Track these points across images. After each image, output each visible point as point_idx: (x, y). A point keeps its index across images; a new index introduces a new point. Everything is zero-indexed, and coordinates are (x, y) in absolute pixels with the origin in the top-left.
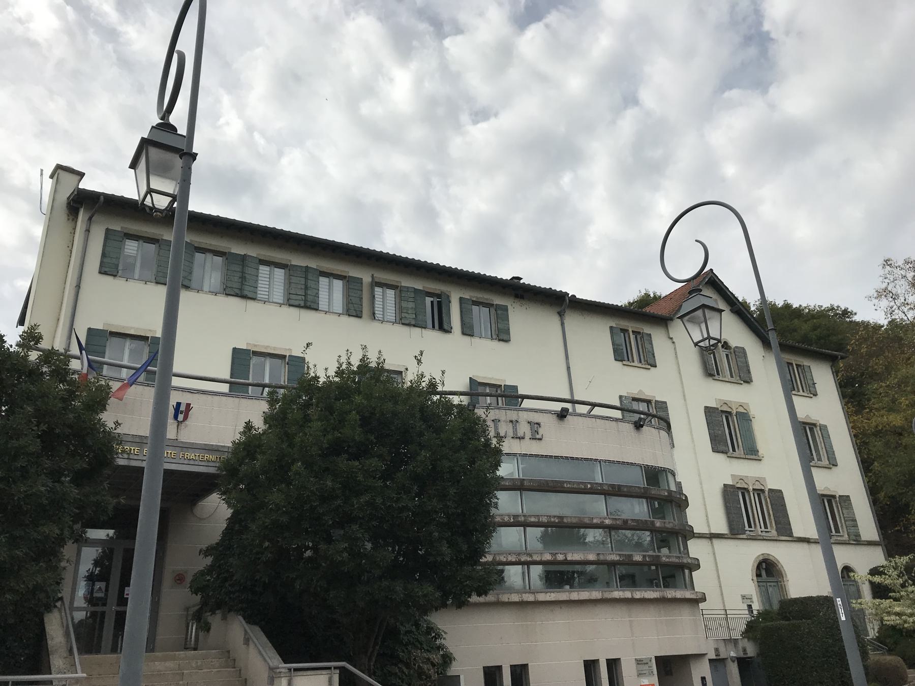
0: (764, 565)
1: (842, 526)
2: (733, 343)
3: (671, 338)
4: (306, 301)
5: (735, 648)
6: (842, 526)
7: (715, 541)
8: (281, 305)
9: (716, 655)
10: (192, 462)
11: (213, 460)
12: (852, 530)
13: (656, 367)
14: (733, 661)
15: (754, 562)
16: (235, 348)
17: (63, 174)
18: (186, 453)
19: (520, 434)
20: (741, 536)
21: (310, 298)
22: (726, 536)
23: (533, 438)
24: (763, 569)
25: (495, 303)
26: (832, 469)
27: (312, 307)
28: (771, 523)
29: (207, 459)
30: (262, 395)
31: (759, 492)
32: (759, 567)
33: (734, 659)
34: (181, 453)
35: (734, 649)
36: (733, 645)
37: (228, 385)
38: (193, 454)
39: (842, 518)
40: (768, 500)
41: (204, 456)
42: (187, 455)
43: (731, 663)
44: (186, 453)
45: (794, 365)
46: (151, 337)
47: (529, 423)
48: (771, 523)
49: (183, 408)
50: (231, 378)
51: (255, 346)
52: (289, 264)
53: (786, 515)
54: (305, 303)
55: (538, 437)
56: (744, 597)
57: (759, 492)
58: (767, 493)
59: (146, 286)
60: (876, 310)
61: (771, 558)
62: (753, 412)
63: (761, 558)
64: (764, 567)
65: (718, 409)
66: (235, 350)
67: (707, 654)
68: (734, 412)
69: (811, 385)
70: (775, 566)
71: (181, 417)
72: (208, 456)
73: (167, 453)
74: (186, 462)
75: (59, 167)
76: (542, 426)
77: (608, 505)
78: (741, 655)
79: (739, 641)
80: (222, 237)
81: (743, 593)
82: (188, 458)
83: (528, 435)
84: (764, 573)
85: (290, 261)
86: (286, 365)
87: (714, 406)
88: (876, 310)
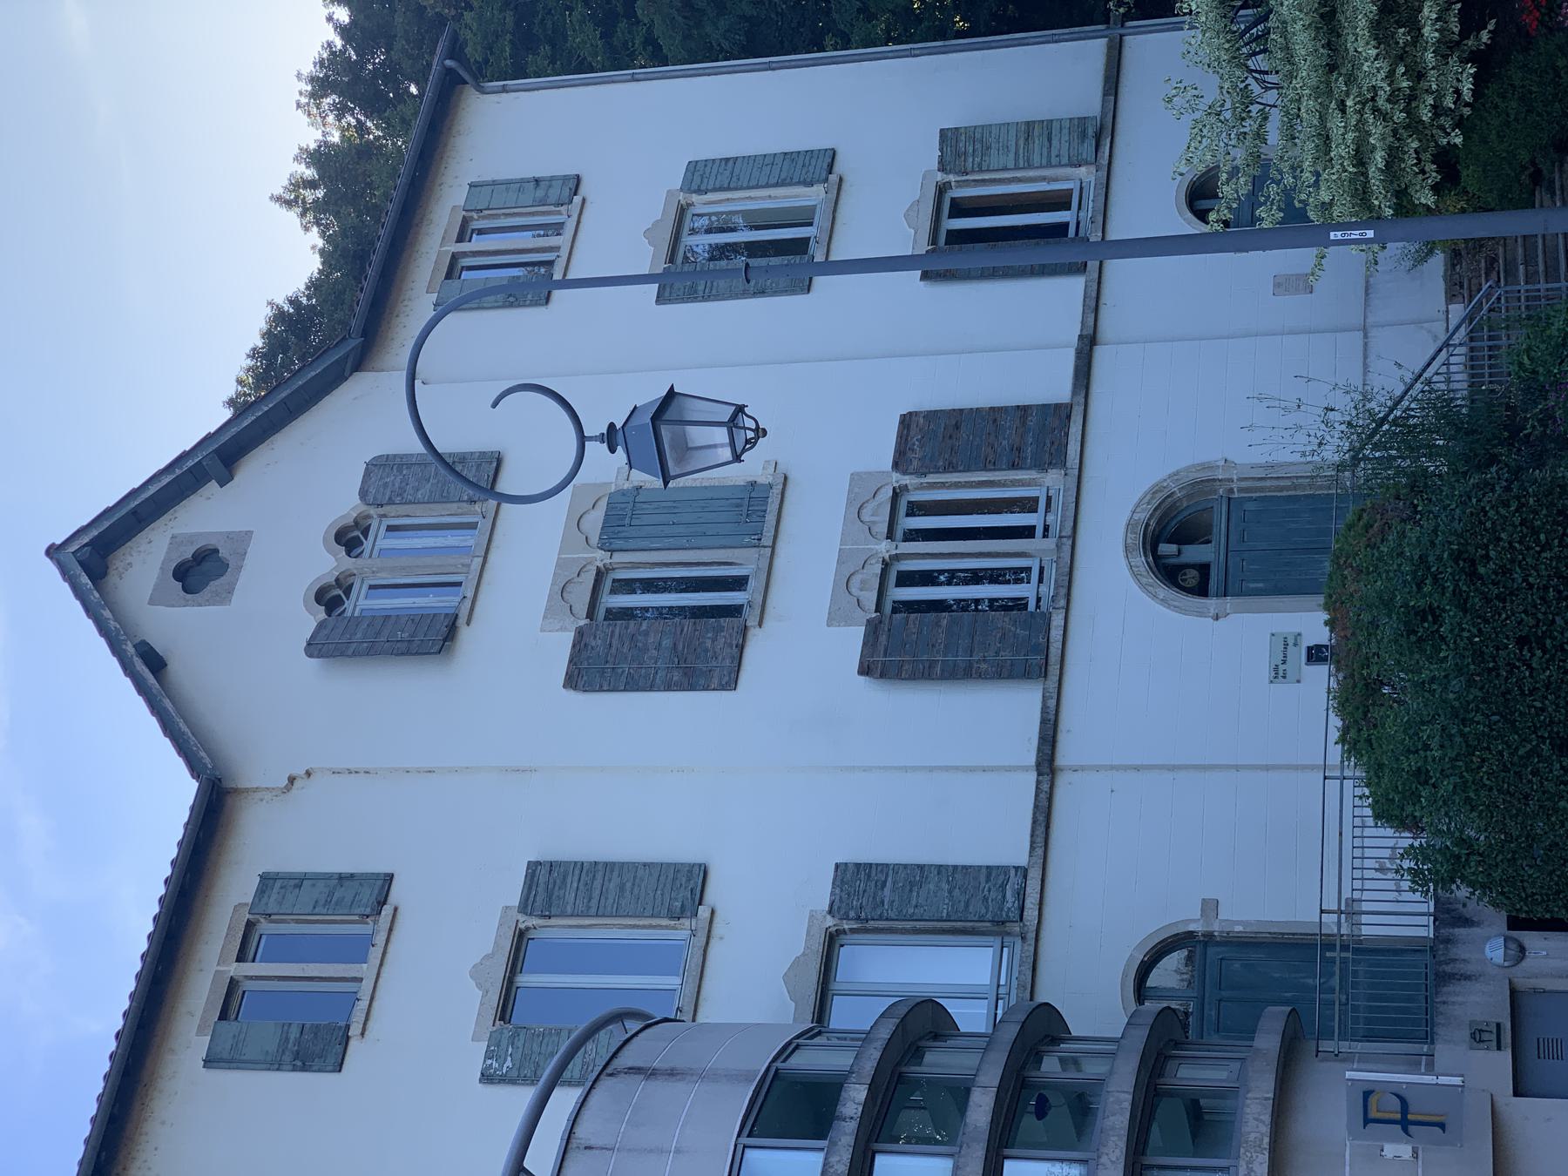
1: (1044, 179)
2: (346, 503)
3: (292, 780)
6: (1044, 179)
7: (1062, 759)
12: (1061, 144)
13: (389, 878)
20: (1056, 634)
31: (903, 509)
32: (1168, 573)
36: (1461, 932)
39: (1019, 174)
40: (932, 478)
45: (464, 247)
53: (994, 415)
56: (1278, 674)
57: (903, 509)
58: (907, 480)
63: (1140, 560)
65: (580, 633)
68: (600, 558)
69: (540, 193)
81: (1265, 672)
84: (1194, 553)
87: (568, 638)
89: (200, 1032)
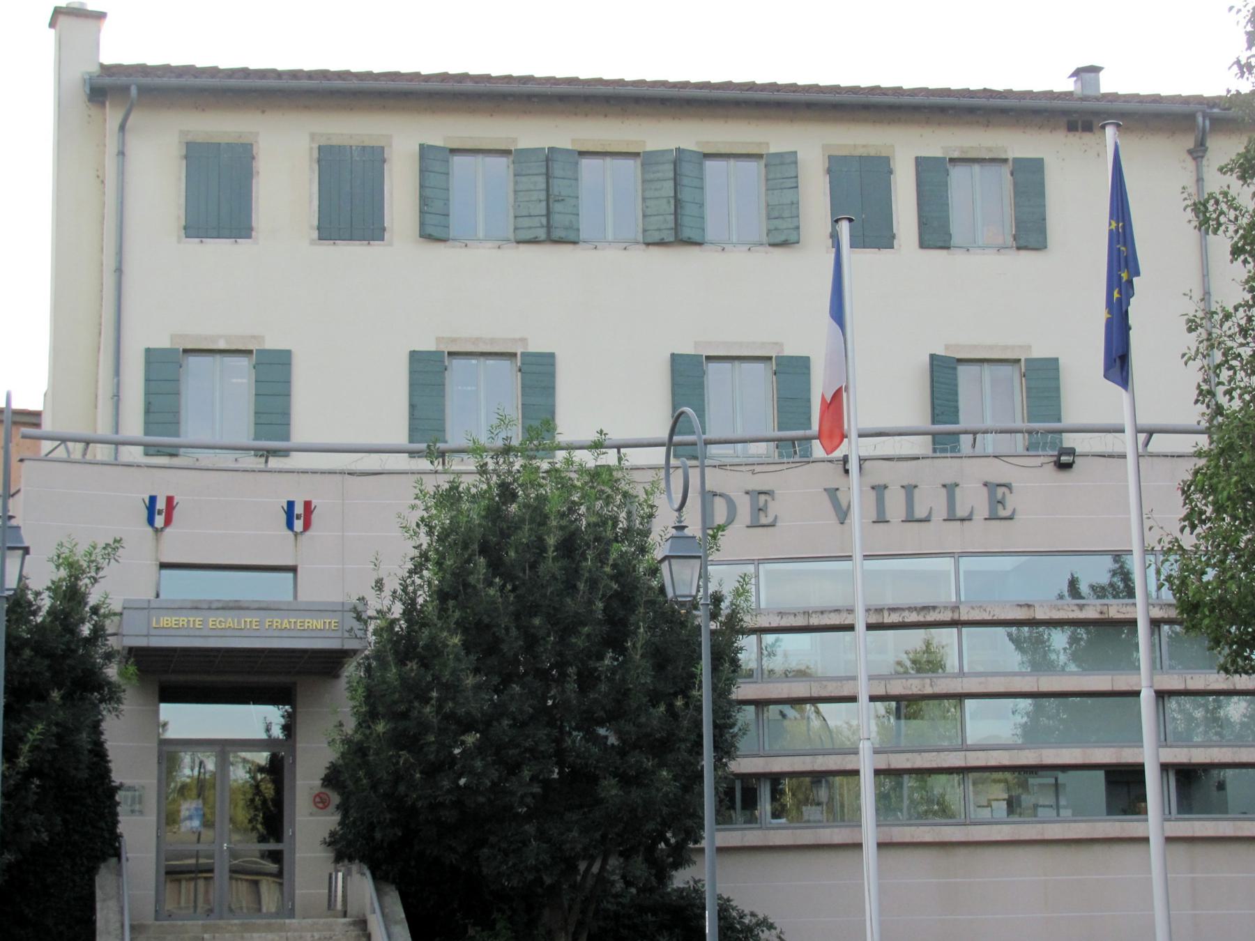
4: (549, 227)
8: (1000, 249)
10: (285, 634)
11: (319, 627)
16: (149, 348)
17: (62, 20)
18: (307, 620)
19: (920, 512)
21: (557, 219)
23: (993, 517)
25: (1011, 155)
26: (1109, 575)
27: (667, 241)
29: (277, 626)
30: (1124, 456)
34: (211, 620)
37: (930, 437)
38: (286, 621)
41: (304, 622)
42: (277, 622)
44: (275, 620)
46: (257, 350)
47: (747, 493)
49: (299, 509)
50: (933, 422)
51: (454, 340)
52: (513, 149)
54: (549, 233)
55: (1002, 513)
62: (147, 347)
66: (415, 356)
71: (159, 521)
72: (279, 621)
73: (245, 622)
74: (276, 634)
75: (58, 12)
76: (1014, 490)
77: (1089, 701)
80: (586, 115)
82: (279, 627)
83: (982, 510)
85: (515, 140)
86: (1023, 379)
88: (1238, 22)
89: (573, 141)
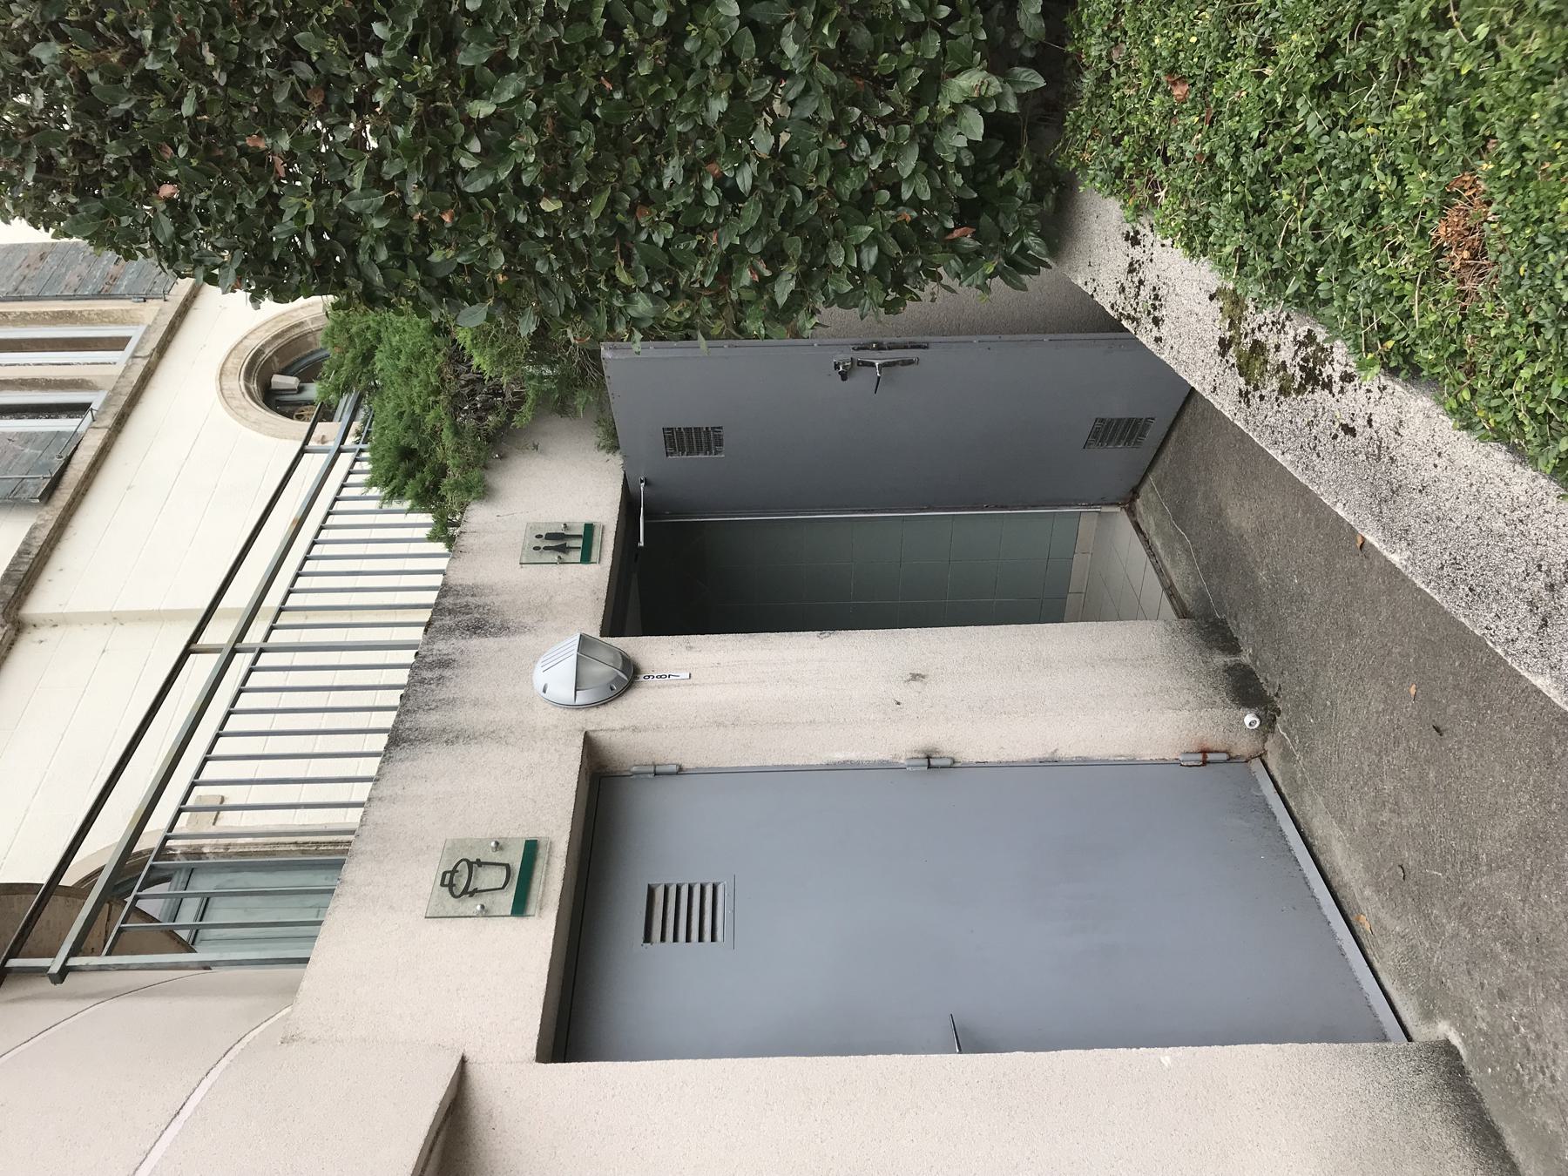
0: (280, 381)
5: (521, 629)
9: (586, 558)
14: (630, 675)
15: (243, 419)
22: (43, 534)
24: (301, 390)
28: (104, 318)
33: (602, 670)
35: (524, 641)
43: (640, 702)
48: (104, 318)
59: (566, 520)
60: (915, 677)
61: (255, 343)
63: (236, 384)
64: (291, 381)
67: (463, 1061)
70: (304, 336)
78: (595, 577)
79: (465, 574)
88: (915, 677)
